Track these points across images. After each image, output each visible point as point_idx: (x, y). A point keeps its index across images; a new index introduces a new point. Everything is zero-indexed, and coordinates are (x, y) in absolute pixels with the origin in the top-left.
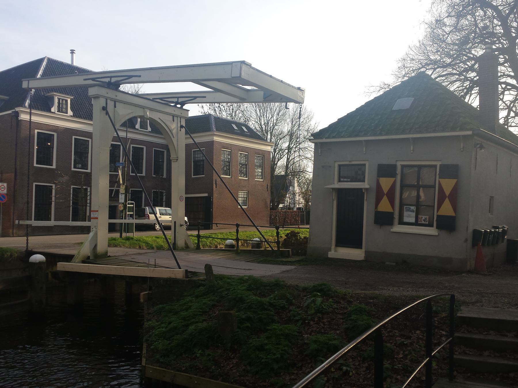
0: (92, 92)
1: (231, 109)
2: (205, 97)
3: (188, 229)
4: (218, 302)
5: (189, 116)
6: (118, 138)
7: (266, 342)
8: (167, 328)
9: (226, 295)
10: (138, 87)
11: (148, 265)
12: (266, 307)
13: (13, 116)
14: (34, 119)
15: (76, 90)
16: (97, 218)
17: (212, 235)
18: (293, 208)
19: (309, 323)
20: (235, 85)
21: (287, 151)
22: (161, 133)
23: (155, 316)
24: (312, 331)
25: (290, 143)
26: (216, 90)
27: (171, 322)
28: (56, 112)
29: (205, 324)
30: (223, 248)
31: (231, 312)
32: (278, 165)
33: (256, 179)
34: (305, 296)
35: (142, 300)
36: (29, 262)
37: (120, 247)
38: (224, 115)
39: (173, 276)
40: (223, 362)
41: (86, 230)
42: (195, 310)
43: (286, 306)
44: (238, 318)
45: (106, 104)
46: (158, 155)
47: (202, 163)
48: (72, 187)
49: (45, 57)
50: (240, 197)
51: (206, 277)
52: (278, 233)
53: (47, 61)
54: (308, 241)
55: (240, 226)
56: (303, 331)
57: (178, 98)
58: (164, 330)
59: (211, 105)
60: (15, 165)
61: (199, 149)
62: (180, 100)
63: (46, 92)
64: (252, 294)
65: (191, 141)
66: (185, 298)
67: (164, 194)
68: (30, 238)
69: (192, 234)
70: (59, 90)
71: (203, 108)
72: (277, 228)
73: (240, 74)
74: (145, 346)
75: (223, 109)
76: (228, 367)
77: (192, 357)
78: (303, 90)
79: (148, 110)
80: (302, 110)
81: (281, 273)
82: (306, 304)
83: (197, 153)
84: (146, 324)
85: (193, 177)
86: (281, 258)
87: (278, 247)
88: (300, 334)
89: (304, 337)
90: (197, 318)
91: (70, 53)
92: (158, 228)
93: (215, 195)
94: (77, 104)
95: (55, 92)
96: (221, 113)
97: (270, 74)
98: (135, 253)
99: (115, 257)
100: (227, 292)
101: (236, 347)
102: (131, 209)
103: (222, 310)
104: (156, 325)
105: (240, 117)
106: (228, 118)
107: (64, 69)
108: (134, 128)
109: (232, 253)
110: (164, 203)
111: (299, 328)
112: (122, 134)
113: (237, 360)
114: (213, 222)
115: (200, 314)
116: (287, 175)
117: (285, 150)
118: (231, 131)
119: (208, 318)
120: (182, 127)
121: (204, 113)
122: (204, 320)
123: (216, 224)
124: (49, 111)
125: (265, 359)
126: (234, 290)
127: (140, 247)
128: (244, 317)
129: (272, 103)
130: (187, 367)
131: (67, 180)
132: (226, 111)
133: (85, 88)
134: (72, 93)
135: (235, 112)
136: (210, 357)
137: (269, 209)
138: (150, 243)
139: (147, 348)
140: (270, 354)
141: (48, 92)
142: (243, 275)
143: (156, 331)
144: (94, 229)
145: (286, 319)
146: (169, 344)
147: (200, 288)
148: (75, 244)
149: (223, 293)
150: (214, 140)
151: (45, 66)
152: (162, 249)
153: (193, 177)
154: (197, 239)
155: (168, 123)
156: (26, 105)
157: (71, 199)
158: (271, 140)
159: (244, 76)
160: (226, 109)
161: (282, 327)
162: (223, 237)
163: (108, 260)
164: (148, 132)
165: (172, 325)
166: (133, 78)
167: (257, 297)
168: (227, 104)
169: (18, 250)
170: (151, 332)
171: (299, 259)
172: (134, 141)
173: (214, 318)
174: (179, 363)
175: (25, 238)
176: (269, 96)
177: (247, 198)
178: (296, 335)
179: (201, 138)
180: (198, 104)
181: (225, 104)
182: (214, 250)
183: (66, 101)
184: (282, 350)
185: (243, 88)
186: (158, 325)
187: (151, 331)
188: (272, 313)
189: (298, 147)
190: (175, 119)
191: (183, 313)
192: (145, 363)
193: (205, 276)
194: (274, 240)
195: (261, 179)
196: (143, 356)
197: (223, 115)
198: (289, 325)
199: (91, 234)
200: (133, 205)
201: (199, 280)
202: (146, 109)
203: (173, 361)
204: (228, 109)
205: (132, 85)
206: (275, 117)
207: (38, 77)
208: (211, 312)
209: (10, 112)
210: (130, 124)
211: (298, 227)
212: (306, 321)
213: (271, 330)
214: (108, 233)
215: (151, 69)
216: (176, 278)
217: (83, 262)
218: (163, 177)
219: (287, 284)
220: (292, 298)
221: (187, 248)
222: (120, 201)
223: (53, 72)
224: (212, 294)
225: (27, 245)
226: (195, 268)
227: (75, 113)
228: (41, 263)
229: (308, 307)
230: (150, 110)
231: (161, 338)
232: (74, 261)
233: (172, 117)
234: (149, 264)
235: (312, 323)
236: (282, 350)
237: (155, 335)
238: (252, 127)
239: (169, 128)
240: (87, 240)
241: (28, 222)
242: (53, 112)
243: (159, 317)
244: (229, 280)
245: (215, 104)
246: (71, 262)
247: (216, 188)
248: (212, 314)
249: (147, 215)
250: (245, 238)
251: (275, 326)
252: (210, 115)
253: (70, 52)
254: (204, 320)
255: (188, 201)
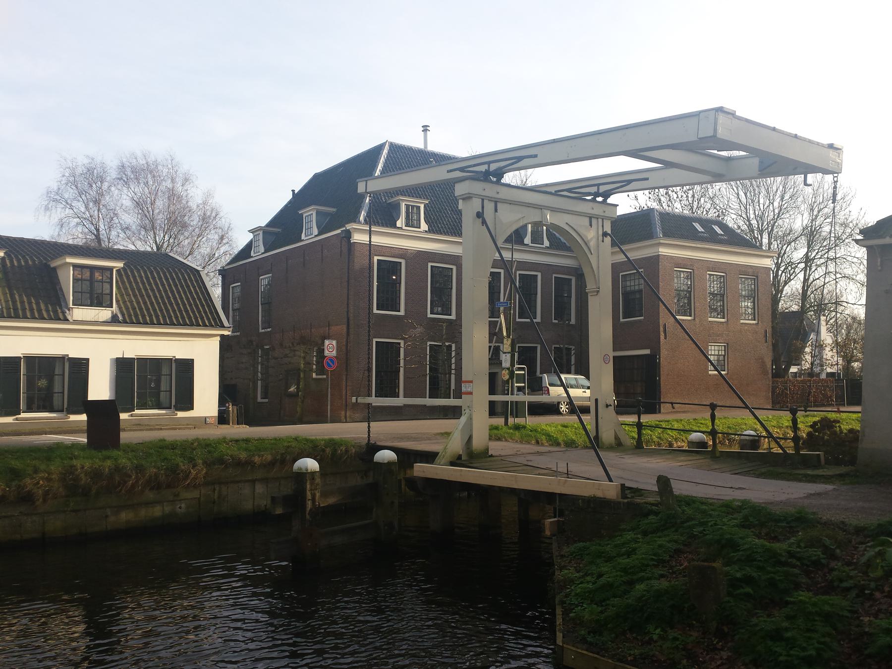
0: (460, 189)
1: (690, 196)
2: (647, 179)
3: (618, 413)
4: (685, 545)
5: (618, 214)
6: (502, 263)
7: (785, 624)
8: (596, 584)
9: (701, 532)
10: (526, 175)
11: (555, 473)
12: (783, 559)
13: (342, 237)
14: (377, 240)
15: (432, 189)
16: (471, 393)
17: (661, 423)
18: (819, 373)
19: (871, 595)
20: (703, 152)
21: (802, 265)
22: (568, 249)
23: (572, 561)
24: (880, 610)
25: (808, 249)
26: (668, 165)
27: (603, 575)
28: (404, 228)
29: (664, 584)
30: (683, 447)
31: (714, 565)
32: (784, 293)
33: (742, 321)
34: (862, 543)
35: (548, 533)
36: (374, 461)
37: (506, 440)
38: (678, 208)
39: (599, 494)
40: (702, 653)
41: (454, 413)
42: (643, 556)
43: (823, 561)
44: (728, 577)
45: (483, 207)
46: (563, 285)
47: (638, 296)
48: (429, 343)
49: (386, 141)
50: (711, 355)
51: (659, 499)
52: (795, 422)
53: (388, 148)
54: (860, 438)
55: (718, 408)
56: (860, 610)
57: (598, 185)
58: (590, 586)
59: (652, 193)
60: (348, 312)
61: (636, 271)
62: (603, 189)
63: (388, 196)
64: (752, 534)
65: (621, 258)
66: (625, 533)
67: (573, 352)
68: (372, 424)
69: (624, 421)
70: (407, 191)
71: (637, 199)
72: (794, 412)
73: (715, 130)
74: (559, 611)
75: (675, 196)
76: (713, 663)
77: (644, 640)
78: (840, 148)
79: (549, 212)
80: (838, 186)
81: (806, 497)
82: (864, 560)
83: (628, 279)
84: (559, 575)
85: (622, 320)
86: (802, 469)
87: (797, 448)
88: (855, 616)
89: (862, 621)
90: (650, 571)
91: (423, 131)
92: (564, 411)
93: (664, 352)
94: (434, 211)
95: (402, 195)
96: (671, 205)
97: (772, 126)
98: (533, 451)
99: (500, 458)
100: (702, 529)
101: (726, 629)
102: (520, 378)
103: (693, 560)
104: (576, 577)
105: (708, 210)
106: (685, 212)
107: (413, 158)
108: (521, 243)
109: (702, 458)
110: (573, 368)
111: (851, 604)
112: (507, 255)
113: (730, 654)
114: (662, 401)
115: (653, 565)
116: (803, 311)
117: (798, 263)
118: (694, 236)
119: (669, 572)
120: (605, 234)
121: (639, 209)
122: (662, 576)
123: (672, 403)
124: (393, 225)
125: (785, 655)
126: (716, 524)
127: (537, 442)
128: (739, 575)
129: (772, 178)
130: (637, 655)
131: (421, 333)
132: (681, 201)
133: (449, 185)
134: (426, 195)
135: (699, 200)
136: (678, 643)
137: (770, 376)
138: (553, 436)
139: (562, 615)
140: (795, 647)
141: (392, 197)
142: (731, 499)
143: (576, 587)
144: (467, 411)
145: (823, 584)
146: (601, 612)
147: (651, 517)
148: (438, 434)
149: (694, 530)
150: (660, 253)
151: (386, 156)
152: (574, 446)
153: (622, 320)
154: (636, 430)
155: (582, 231)
156: (360, 219)
157: (428, 363)
158: (770, 248)
159: (722, 133)
160: (680, 196)
161: (816, 600)
162: (681, 427)
163: (491, 461)
164: (544, 248)
165: (603, 580)
166: (525, 160)
167: (762, 540)
168: (683, 188)
169: (355, 443)
170: (569, 588)
171: (842, 472)
172: (522, 265)
173: (680, 573)
174: (621, 648)
175: (366, 424)
176: (769, 166)
177: (726, 356)
178: (847, 617)
179: (638, 252)
180: (627, 193)
181: (678, 188)
182: (668, 451)
183: (418, 208)
184: (819, 643)
185: (719, 156)
186: (580, 578)
187: (569, 587)
188: (796, 571)
189: (826, 256)
190: (594, 221)
191: (623, 559)
192: (563, 641)
193: (659, 497)
194: (783, 435)
195: (751, 320)
196: (557, 628)
197: (675, 208)
198: (832, 597)
199: (463, 419)
200: (524, 371)
201: (646, 503)
202: (545, 210)
203: (610, 643)
204: (685, 196)
205: (517, 172)
206: (776, 204)
207: (376, 175)
208: (674, 563)
209: (339, 231)
210: (517, 237)
211: (836, 410)
212: (867, 592)
213: (793, 603)
214: (489, 418)
215: (554, 141)
216: (605, 498)
217: (452, 464)
218: (571, 323)
219: (821, 518)
220: (835, 546)
221: (618, 445)
222: (504, 365)
223: (398, 165)
224: (673, 529)
225: (369, 435)
226: (636, 481)
227: (431, 226)
228: (390, 464)
229: (869, 564)
230: (551, 210)
231: (586, 601)
232: (438, 462)
233: (587, 220)
234: (558, 471)
235: (878, 595)
236: (819, 643)
237: (577, 595)
238: (731, 224)
239: (583, 240)
240: (457, 429)
241: (368, 400)
242: (400, 227)
243: (580, 564)
244: (704, 507)
245: (660, 189)
246: (433, 463)
247: (665, 338)
248: (676, 566)
249: (546, 389)
250: (725, 430)
251: (803, 596)
252: (650, 211)
253: (422, 129)
254: (662, 576)
255: (619, 364)
